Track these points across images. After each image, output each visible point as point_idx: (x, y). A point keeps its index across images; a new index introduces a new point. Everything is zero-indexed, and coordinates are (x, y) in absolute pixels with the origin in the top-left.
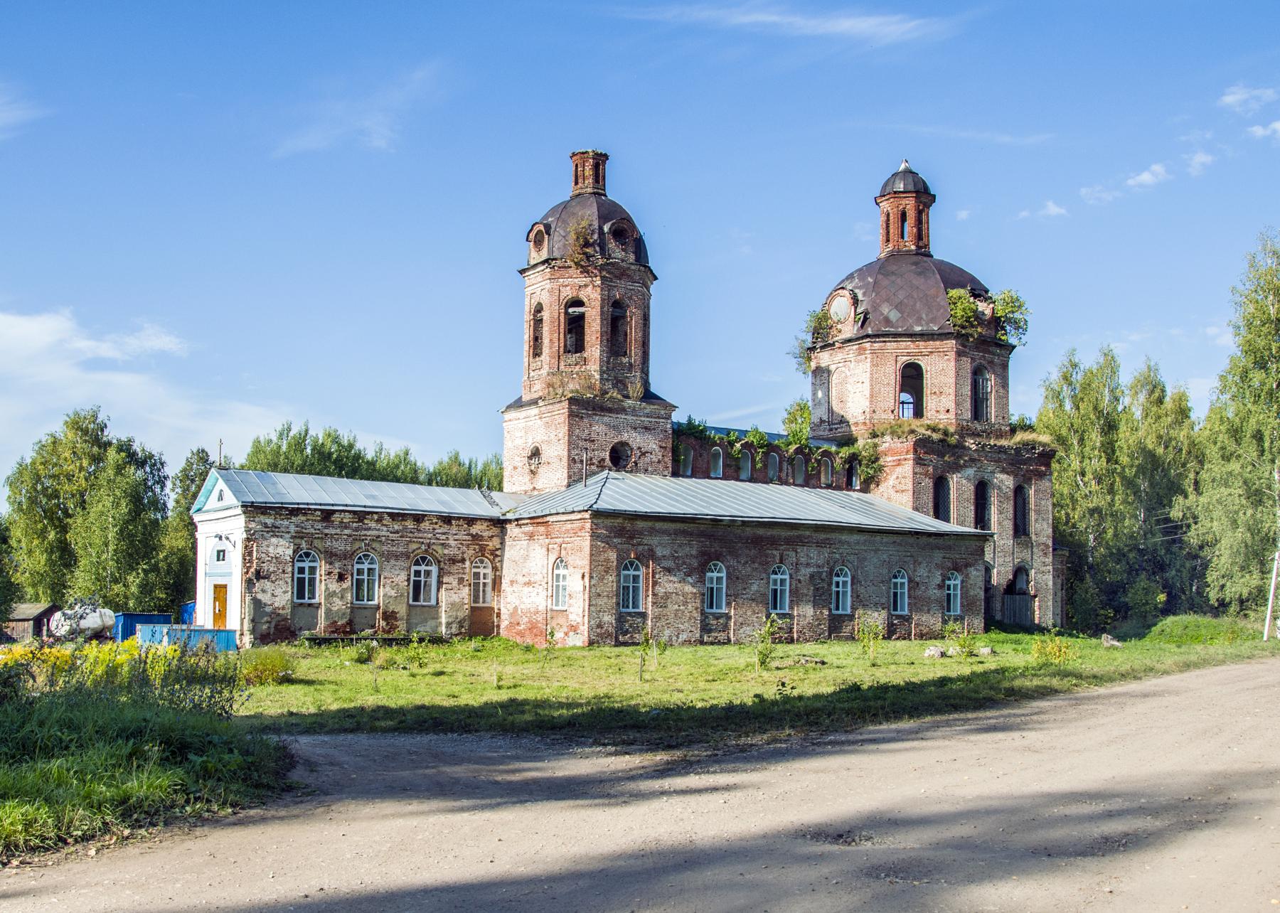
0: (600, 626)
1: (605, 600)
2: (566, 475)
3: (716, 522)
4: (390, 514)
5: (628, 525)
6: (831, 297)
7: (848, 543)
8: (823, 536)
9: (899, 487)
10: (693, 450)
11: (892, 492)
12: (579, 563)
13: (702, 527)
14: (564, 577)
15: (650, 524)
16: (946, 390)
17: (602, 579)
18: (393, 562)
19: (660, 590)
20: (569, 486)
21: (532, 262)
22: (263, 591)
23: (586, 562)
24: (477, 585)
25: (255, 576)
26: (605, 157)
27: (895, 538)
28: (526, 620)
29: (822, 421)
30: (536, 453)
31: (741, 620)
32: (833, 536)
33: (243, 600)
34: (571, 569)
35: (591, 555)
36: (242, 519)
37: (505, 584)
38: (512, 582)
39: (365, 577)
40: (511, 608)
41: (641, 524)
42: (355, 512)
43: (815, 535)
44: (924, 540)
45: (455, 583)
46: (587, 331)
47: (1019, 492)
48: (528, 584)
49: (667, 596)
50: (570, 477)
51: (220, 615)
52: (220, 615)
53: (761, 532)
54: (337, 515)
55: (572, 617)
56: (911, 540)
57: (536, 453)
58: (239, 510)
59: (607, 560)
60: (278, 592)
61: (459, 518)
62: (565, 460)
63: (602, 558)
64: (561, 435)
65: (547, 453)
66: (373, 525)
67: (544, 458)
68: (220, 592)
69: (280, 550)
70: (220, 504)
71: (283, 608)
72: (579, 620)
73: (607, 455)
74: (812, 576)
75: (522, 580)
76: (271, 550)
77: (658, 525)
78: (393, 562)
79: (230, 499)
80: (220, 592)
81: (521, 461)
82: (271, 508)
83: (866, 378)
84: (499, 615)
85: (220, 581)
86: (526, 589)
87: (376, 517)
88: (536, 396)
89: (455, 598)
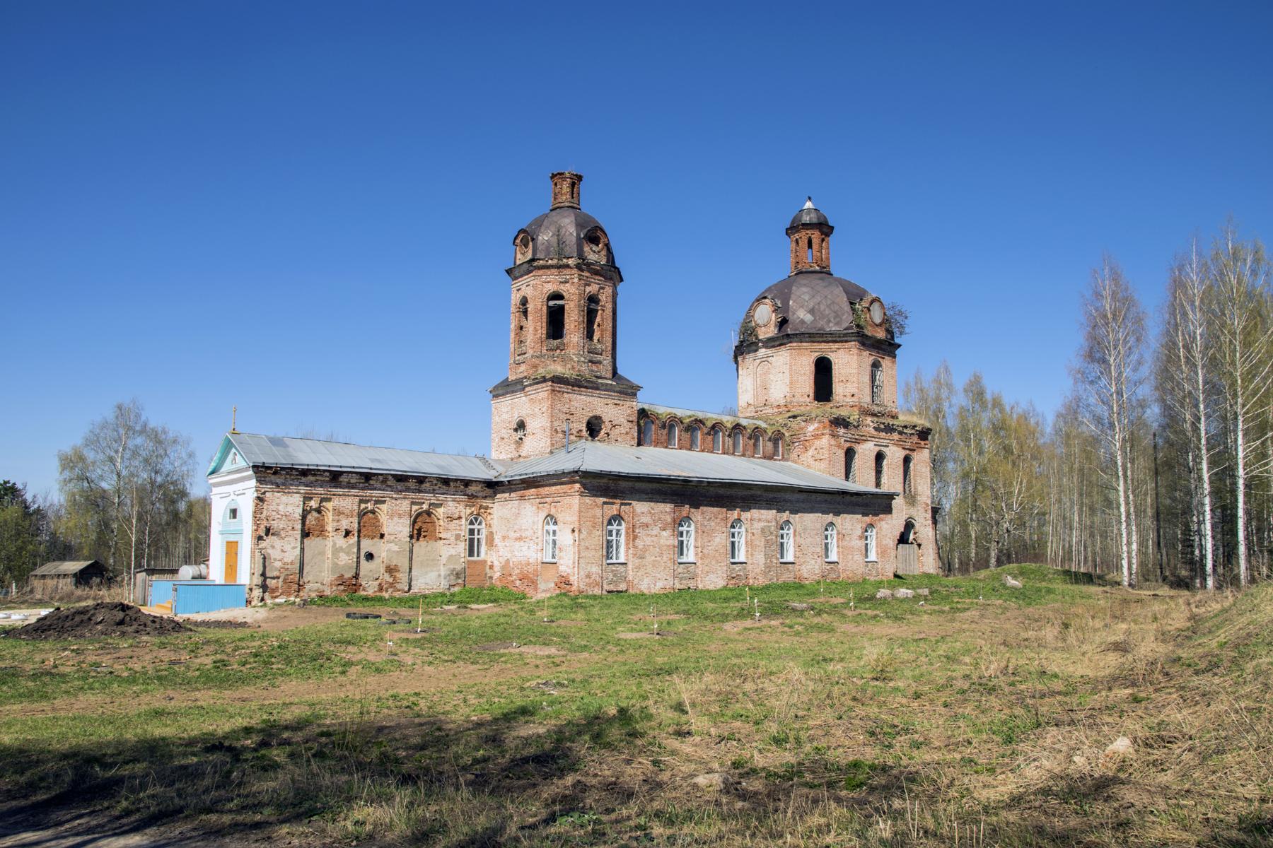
0: (588, 576)
1: (593, 552)
2: (549, 443)
3: (686, 482)
4: (394, 476)
5: (612, 484)
6: (752, 308)
7: (790, 501)
8: (771, 496)
9: (818, 457)
10: (647, 426)
11: (811, 461)
12: (568, 519)
13: (674, 487)
14: (554, 532)
15: (630, 484)
16: (851, 379)
17: (590, 533)
18: (396, 519)
19: (639, 543)
20: (551, 452)
21: (518, 262)
22: (273, 547)
23: (575, 518)
24: (472, 541)
25: (265, 532)
26: (580, 178)
27: (826, 497)
28: (517, 571)
29: (749, 405)
30: (521, 426)
31: (707, 569)
32: (779, 495)
33: (253, 556)
34: (560, 525)
35: (580, 511)
36: (253, 482)
37: (497, 540)
38: (504, 538)
39: (614, 537)
40: (503, 560)
41: (623, 484)
42: (361, 474)
43: (765, 494)
44: (848, 498)
45: (453, 539)
46: (567, 321)
47: (907, 460)
48: (520, 539)
49: (645, 549)
50: (552, 445)
51: (231, 568)
52: (231, 568)
53: (722, 491)
54: (345, 475)
55: (562, 568)
56: (839, 498)
57: (521, 426)
58: (251, 472)
59: (594, 516)
60: (287, 547)
61: (456, 480)
62: (548, 430)
63: (590, 514)
64: (544, 409)
65: (531, 425)
66: (378, 485)
67: (529, 429)
68: (232, 549)
69: (290, 509)
70: (235, 467)
71: (292, 563)
72: (569, 571)
73: (584, 427)
74: (763, 530)
75: (512, 535)
76: (281, 508)
77: (638, 485)
78: (396, 519)
79: (241, 463)
80: (232, 549)
81: (508, 433)
82: (282, 469)
83: (786, 369)
84: (491, 567)
85: (232, 538)
86: (518, 544)
87: (381, 478)
88: (521, 376)
89: (453, 552)
